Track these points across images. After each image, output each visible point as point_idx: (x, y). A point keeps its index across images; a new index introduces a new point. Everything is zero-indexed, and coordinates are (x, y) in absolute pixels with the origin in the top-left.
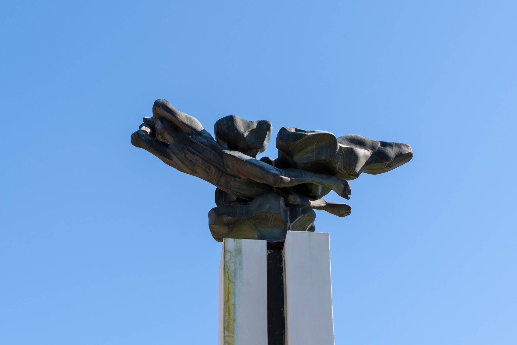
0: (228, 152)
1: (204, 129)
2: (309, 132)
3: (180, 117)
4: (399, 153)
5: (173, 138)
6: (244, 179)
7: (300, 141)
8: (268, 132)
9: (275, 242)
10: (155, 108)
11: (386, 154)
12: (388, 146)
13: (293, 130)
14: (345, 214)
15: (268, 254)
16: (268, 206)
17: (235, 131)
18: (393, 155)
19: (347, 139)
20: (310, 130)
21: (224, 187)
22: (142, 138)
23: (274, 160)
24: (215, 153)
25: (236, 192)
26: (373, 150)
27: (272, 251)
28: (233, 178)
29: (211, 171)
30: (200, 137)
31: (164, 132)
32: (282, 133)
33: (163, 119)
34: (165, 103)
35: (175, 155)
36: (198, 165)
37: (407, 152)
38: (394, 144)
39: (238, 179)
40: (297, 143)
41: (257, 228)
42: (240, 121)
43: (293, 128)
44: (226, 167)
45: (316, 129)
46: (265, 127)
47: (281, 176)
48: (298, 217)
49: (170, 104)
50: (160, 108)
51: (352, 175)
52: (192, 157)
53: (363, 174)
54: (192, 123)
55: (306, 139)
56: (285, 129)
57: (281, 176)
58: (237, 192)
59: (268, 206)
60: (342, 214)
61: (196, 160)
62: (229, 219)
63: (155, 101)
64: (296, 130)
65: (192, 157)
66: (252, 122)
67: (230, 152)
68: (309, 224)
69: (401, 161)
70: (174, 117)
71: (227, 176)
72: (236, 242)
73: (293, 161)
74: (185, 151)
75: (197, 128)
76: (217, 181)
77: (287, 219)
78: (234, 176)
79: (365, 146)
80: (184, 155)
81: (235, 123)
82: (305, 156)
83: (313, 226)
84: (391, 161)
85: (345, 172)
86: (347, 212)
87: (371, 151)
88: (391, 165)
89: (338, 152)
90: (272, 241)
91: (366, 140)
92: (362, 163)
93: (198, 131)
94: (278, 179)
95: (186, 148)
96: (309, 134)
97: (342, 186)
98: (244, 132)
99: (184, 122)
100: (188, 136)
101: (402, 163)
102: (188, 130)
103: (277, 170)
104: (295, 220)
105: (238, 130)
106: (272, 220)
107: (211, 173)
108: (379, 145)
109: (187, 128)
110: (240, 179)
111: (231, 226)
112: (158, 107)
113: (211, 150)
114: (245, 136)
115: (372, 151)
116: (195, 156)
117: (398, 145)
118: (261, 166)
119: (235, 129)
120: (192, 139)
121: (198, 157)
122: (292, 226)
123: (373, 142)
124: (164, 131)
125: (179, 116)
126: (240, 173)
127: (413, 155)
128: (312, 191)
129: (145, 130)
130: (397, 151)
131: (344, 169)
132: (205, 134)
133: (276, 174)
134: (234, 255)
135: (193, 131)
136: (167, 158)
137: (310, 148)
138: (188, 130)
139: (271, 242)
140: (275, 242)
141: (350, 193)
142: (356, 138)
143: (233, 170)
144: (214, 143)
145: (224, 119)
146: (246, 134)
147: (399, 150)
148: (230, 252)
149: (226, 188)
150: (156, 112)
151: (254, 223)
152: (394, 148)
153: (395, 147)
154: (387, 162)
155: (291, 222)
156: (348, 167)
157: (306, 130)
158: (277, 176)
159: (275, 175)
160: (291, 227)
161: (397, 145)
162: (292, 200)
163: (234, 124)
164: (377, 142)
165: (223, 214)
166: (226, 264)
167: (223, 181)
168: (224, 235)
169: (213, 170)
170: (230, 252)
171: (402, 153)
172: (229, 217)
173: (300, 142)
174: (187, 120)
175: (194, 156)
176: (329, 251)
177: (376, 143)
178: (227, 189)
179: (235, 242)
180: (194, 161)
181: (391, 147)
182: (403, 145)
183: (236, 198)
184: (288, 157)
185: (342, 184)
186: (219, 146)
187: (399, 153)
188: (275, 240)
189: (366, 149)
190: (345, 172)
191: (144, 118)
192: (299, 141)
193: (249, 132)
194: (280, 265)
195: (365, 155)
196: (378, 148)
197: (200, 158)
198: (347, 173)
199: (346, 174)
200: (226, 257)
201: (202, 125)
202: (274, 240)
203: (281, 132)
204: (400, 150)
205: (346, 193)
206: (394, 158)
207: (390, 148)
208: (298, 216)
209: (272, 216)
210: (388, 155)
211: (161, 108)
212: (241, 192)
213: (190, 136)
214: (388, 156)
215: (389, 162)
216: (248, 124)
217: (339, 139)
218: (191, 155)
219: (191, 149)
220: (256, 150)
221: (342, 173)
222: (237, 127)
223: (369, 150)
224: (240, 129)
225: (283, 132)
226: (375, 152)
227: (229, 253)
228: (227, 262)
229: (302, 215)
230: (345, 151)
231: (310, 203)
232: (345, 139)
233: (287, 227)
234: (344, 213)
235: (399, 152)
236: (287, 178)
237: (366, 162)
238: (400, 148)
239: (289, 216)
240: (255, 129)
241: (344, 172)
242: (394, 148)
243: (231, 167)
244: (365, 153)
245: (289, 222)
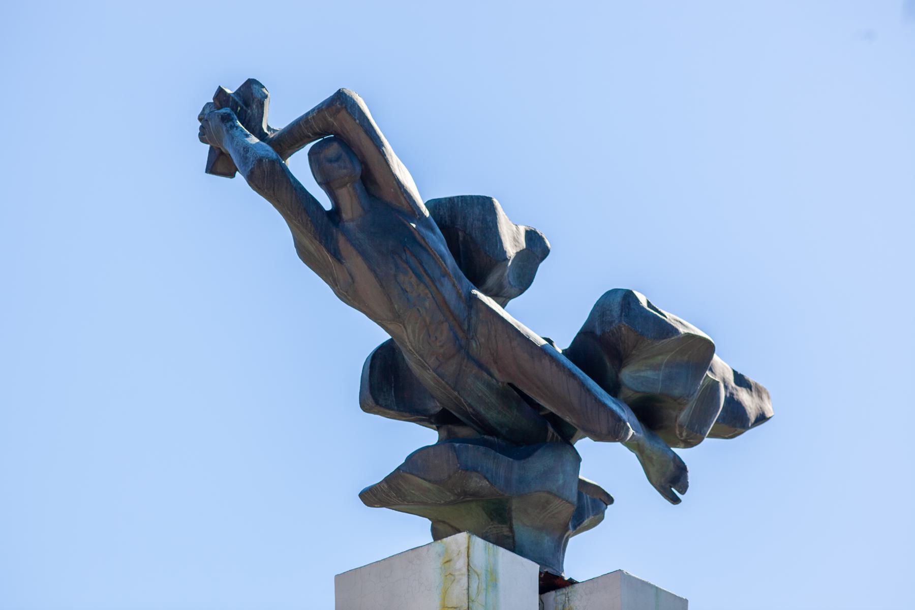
21: (447, 383)
28: (475, 370)
31: (345, 185)
39: (485, 375)
45: (664, 310)
48: (585, 519)
61: (419, 296)
62: (482, 486)
64: (649, 304)
71: (466, 360)
73: (617, 377)
82: (642, 374)
110: (490, 378)
124: (347, 183)
127: (234, 178)
131: (687, 427)
141: (683, 490)
145: (475, 201)
149: (450, 386)
158: (622, 423)
166: (470, 604)
175: (418, 285)
178: (453, 389)
183: (438, 409)
184: (608, 364)
191: (220, 86)
200: (470, 585)
212: (481, 409)
219: (412, 260)
228: (473, 601)
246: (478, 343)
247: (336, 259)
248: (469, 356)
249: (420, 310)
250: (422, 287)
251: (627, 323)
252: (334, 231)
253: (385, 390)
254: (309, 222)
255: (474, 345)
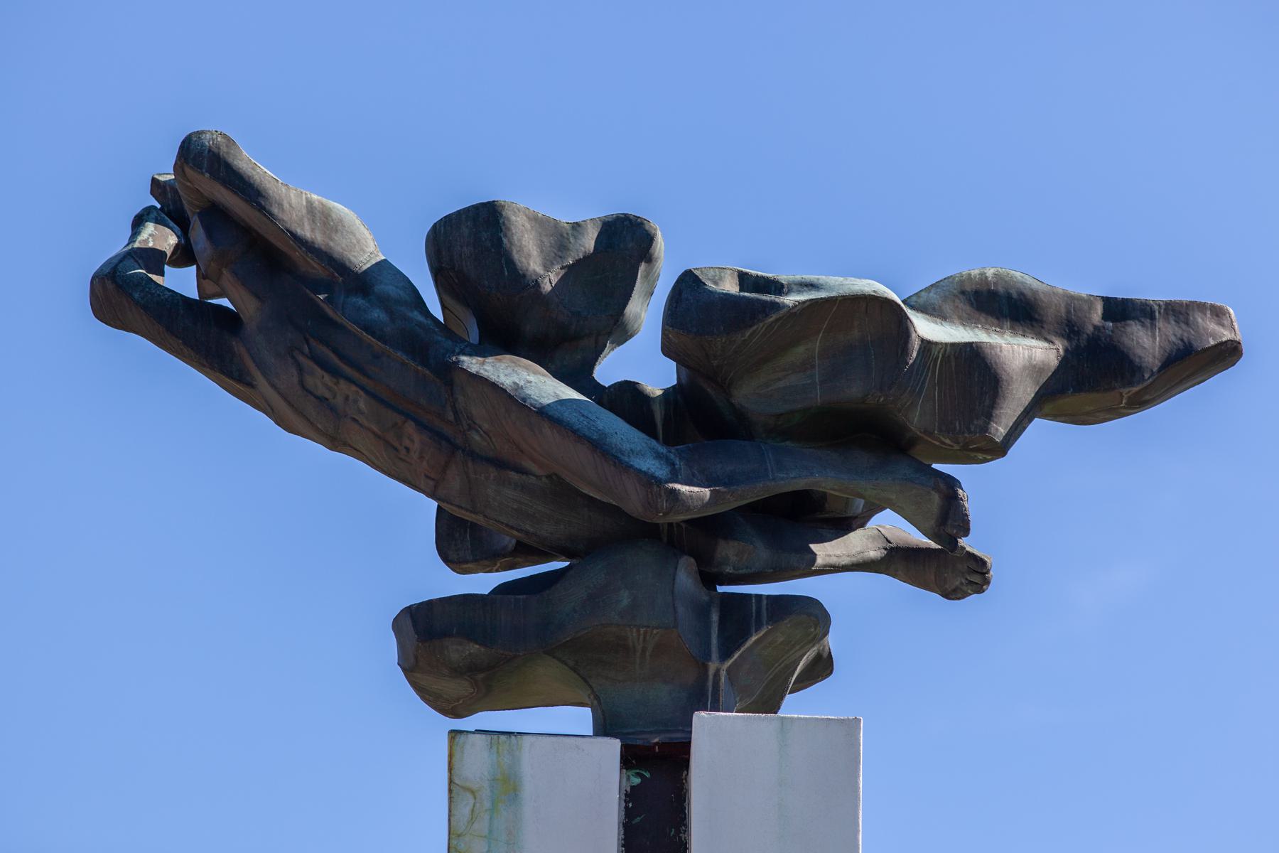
0: (472, 364)
1: (383, 258)
2: (795, 287)
3: (283, 210)
4: (1182, 347)
5: (257, 297)
6: (536, 476)
7: (754, 331)
8: (643, 267)
9: (656, 740)
10: (183, 171)
11: (1123, 352)
12: (1133, 319)
13: (730, 286)
14: (965, 588)
15: (632, 788)
16: (625, 599)
17: (506, 273)
18: (1154, 357)
19: (963, 293)
20: (798, 277)
22: (131, 294)
23: (659, 393)
24: (419, 368)
25: (507, 525)
26: (1069, 338)
27: (647, 775)
28: (493, 472)
29: (407, 442)
30: (360, 301)
31: (221, 273)
32: (684, 295)
33: (215, 215)
34: (224, 149)
35: (264, 374)
36: (354, 420)
37: (1212, 342)
38: (1159, 305)
40: (744, 340)
41: (586, 681)
42: (528, 226)
43: (729, 272)
44: (466, 427)
46: (631, 245)
47: (671, 485)
48: (751, 635)
49: (244, 153)
50: (203, 174)
51: (979, 450)
52: (329, 389)
53: (1039, 427)
54: (334, 236)
55: (777, 320)
56: (697, 277)
57: (671, 485)
58: (512, 528)
59: (625, 599)
60: (953, 587)
61: (347, 398)
62: (470, 654)
63: (184, 142)
64: (744, 279)
65: (329, 389)
66: (576, 226)
67: (483, 364)
68: (801, 653)
69: (1188, 377)
70: (257, 214)
71: (470, 464)
72: (498, 748)
73: (732, 404)
74: (301, 359)
75: (353, 259)
76: (432, 483)
77: (709, 644)
78: (500, 464)
79: (1036, 320)
80: (295, 380)
81: (506, 236)
82: (781, 384)
83: (825, 655)
84: (1145, 384)
85: (948, 441)
86: (971, 583)
87: (1060, 345)
88: (1147, 397)
89: (912, 365)
90: (644, 736)
91: (1042, 296)
92: (1020, 393)
93: (357, 273)
94: (661, 496)
95: (306, 350)
96: (790, 300)
97: (936, 498)
98: (542, 272)
99: (299, 231)
100: (312, 295)
101: (1204, 377)
102: (315, 266)
103: (658, 456)
104: (738, 648)
105: (518, 263)
106: (644, 650)
107: (407, 449)
108: (1097, 316)
109: (313, 259)
110: (524, 477)
111: (480, 676)
112: (191, 168)
113: (404, 357)
114: (547, 287)
115: (1066, 343)
116: (342, 382)
117: (1179, 312)
118: (595, 437)
119: (503, 262)
120: (329, 311)
121: (354, 388)
122: (729, 671)
123: (1073, 302)
124: (220, 270)
125: (280, 205)
126: (522, 451)
128: (827, 505)
129: (151, 245)
130: (1173, 338)
131: (940, 430)
132: (387, 288)
133: (653, 477)
134: (487, 805)
135: (337, 275)
136: (232, 378)
137: (800, 351)
138: (314, 268)
139: (639, 742)
140: (657, 744)
142: (1001, 290)
143: (494, 440)
144: (420, 325)
146: (550, 279)
147: (1179, 332)
148: (473, 792)
149: (467, 510)
150: (189, 184)
151: (571, 663)
152: (1161, 325)
153: (1167, 320)
154: (1126, 390)
155: (725, 655)
156: (957, 424)
157: (784, 278)
159: (649, 481)
160: (723, 674)
161: (1173, 310)
162: (733, 559)
163: (500, 240)
164: (1090, 301)
165: (445, 634)
166: (454, 842)
167: (454, 481)
168: (461, 702)
169: (415, 439)
170: (473, 792)
171: (1195, 344)
172: (471, 644)
173: (751, 334)
174: (313, 221)
175: (337, 384)
176: (857, 797)
177: (1086, 307)
179: (495, 749)
180: (339, 401)
181: (1148, 322)
182: (1201, 307)
185: (933, 493)
186: (440, 338)
187: (1182, 347)
188: (658, 732)
189: (1040, 336)
190: (948, 441)
191: (154, 181)
192: (751, 330)
193: (563, 272)
194: (678, 832)
195: (1034, 366)
196: (1090, 329)
197: (361, 393)
198: (958, 443)
199: (952, 446)
201: (376, 238)
202: (651, 732)
203: (680, 293)
204: (1185, 334)
205: (949, 530)
206: (1159, 370)
207: (1143, 325)
208: (754, 634)
209: (641, 637)
210: (1132, 357)
211: (207, 175)
213: (321, 297)
214: (1131, 362)
215: (1135, 389)
216: (562, 236)
217: (931, 294)
218: (327, 378)
220: (596, 342)
221: (938, 443)
222: (514, 252)
223: (1054, 339)
224: (523, 260)
225: (689, 283)
226: (1078, 346)
227: (469, 796)
229: (767, 624)
230: (946, 359)
231: (813, 556)
232: (955, 296)
233: (708, 676)
234: (962, 584)
235: (1182, 340)
236: (696, 489)
237: (1037, 394)
238: (1187, 323)
239: (716, 629)
240: (587, 258)
241: (944, 443)
242: (1160, 323)
243: (486, 426)
244: (1030, 358)
245: (715, 655)
246: (482, 433)
247: (244, 383)
248: (473, 455)
249: (357, 418)
250: (343, 384)
251: (670, 327)
252: (234, 343)
253: (457, 535)
254: (182, 347)
255: (477, 438)
